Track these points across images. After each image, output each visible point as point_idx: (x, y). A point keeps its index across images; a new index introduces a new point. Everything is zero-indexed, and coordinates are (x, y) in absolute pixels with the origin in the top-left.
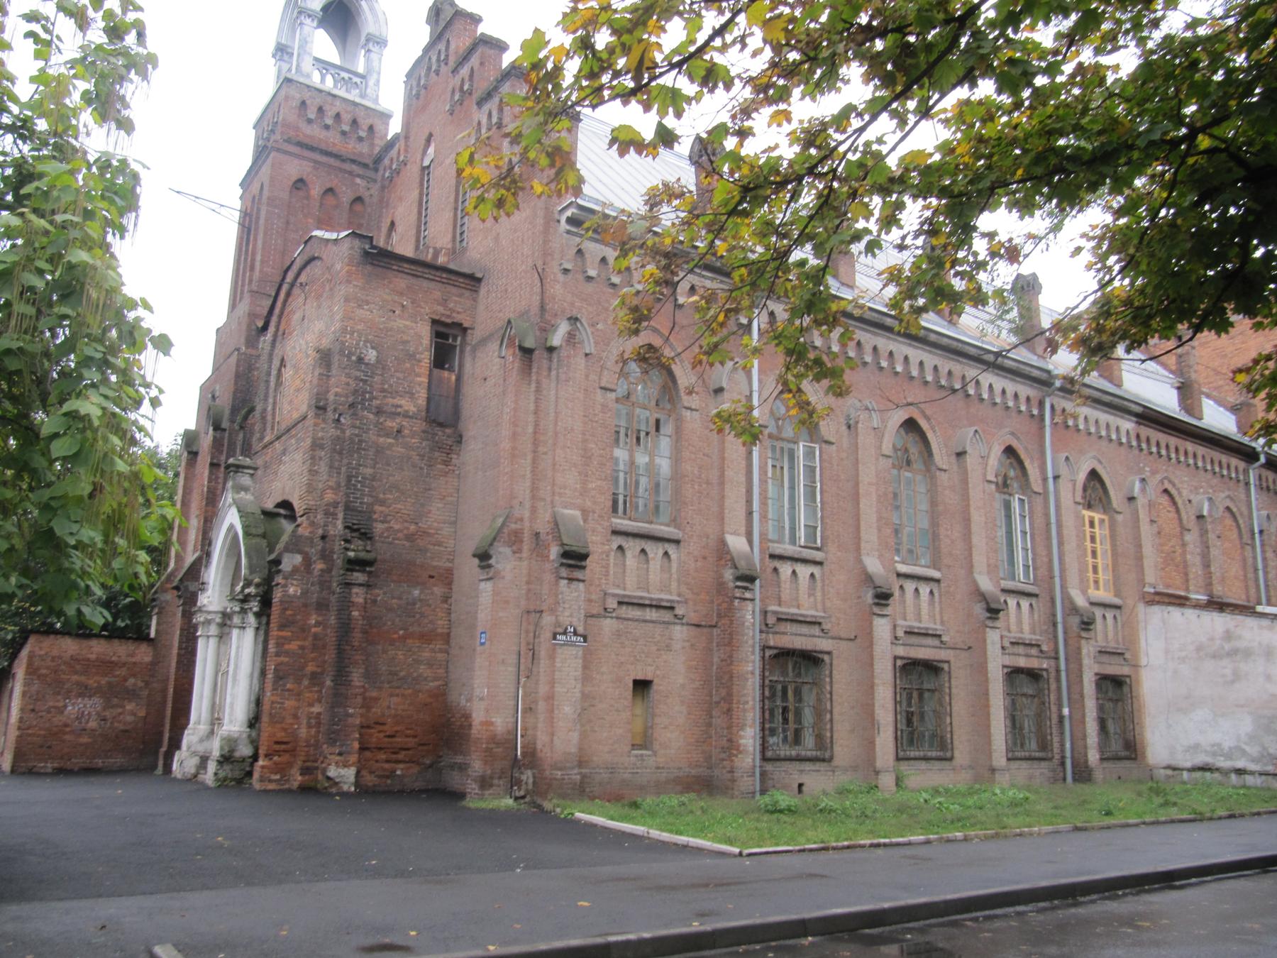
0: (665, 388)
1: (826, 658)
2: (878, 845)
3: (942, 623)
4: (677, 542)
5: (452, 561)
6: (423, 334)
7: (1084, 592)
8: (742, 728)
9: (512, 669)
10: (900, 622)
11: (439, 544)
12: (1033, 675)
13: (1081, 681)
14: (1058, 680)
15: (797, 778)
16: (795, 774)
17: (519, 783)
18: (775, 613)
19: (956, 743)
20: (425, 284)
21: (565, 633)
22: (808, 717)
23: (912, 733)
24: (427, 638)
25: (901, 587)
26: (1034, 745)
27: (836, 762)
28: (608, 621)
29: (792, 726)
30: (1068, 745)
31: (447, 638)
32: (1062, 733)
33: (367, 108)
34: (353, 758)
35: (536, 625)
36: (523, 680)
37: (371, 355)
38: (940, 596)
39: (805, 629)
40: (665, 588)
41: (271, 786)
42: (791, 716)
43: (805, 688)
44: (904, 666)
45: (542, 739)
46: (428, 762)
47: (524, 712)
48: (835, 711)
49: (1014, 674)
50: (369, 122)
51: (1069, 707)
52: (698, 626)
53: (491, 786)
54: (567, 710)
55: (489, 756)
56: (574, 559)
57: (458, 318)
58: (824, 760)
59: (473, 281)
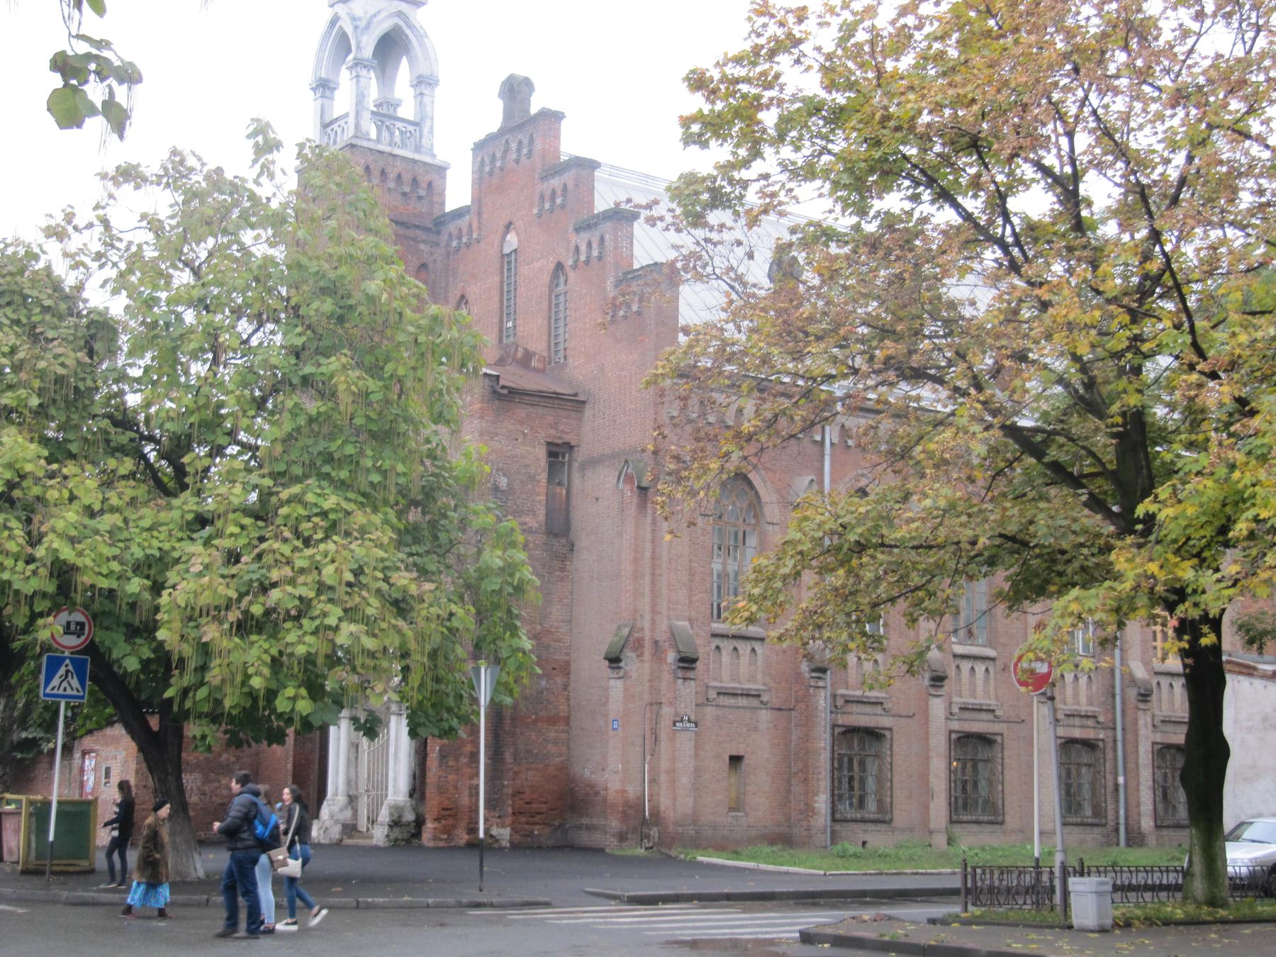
0: (750, 506)
1: (887, 733)
2: (917, 874)
3: (997, 698)
4: (762, 640)
5: (568, 654)
6: (542, 453)
7: (1146, 663)
8: (816, 794)
9: (639, 749)
10: (956, 699)
11: (559, 640)
12: (1089, 745)
13: (1137, 751)
14: (1115, 749)
15: (862, 837)
16: (860, 832)
17: (648, 837)
18: (843, 696)
19: (1007, 809)
20: (541, 411)
21: (682, 721)
22: (871, 784)
23: (965, 800)
24: (553, 720)
25: (958, 667)
26: (1088, 811)
27: (896, 823)
28: (709, 709)
29: (857, 793)
30: (1122, 812)
31: (567, 720)
32: (1117, 801)
33: (425, 164)
34: (508, 820)
35: (657, 714)
36: (648, 758)
37: (503, 482)
38: (995, 673)
39: (868, 709)
40: (752, 679)
41: (441, 844)
42: (856, 785)
43: (869, 761)
44: (959, 739)
45: (665, 803)
46: (557, 824)
47: (651, 782)
48: (895, 780)
49: (1068, 744)
50: (428, 178)
51: (1125, 775)
52: (779, 709)
53: (627, 839)
54: (685, 781)
55: (624, 816)
56: (687, 662)
57: (567, 438)
58: (884, 822)
59: (574, 403)
